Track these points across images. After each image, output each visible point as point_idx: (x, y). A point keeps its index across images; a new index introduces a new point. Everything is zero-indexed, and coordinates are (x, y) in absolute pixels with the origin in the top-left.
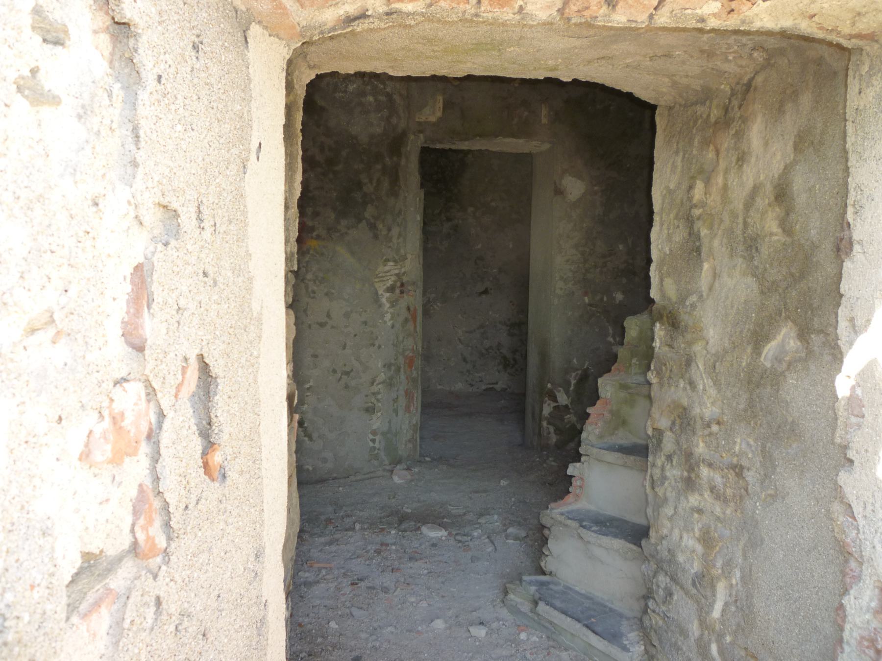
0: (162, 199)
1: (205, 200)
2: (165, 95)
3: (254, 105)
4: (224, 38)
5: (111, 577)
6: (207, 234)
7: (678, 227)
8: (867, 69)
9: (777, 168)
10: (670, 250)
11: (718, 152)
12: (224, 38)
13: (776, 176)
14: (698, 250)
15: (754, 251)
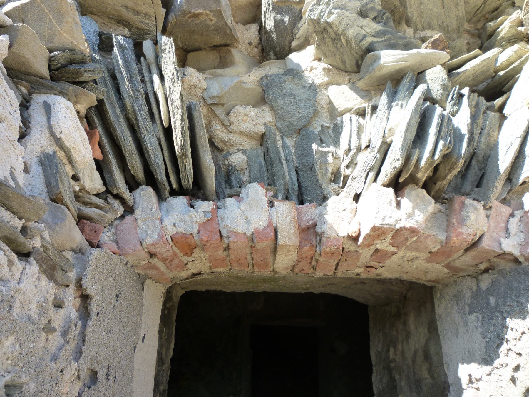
0: (91, 367)
1: (111, 366)
2: (99, 321)
3: (143, 316)
4: (131, 289)
5: (163, 61)
6: (111, 382)
7: (385, 374)
8: (439, 296)
9: (423, 341)
10: (382, 388)
11: (397, 332)
12: (131, 289)
13: (423, 345)
14: (395, 387)
15: (419, 388)
